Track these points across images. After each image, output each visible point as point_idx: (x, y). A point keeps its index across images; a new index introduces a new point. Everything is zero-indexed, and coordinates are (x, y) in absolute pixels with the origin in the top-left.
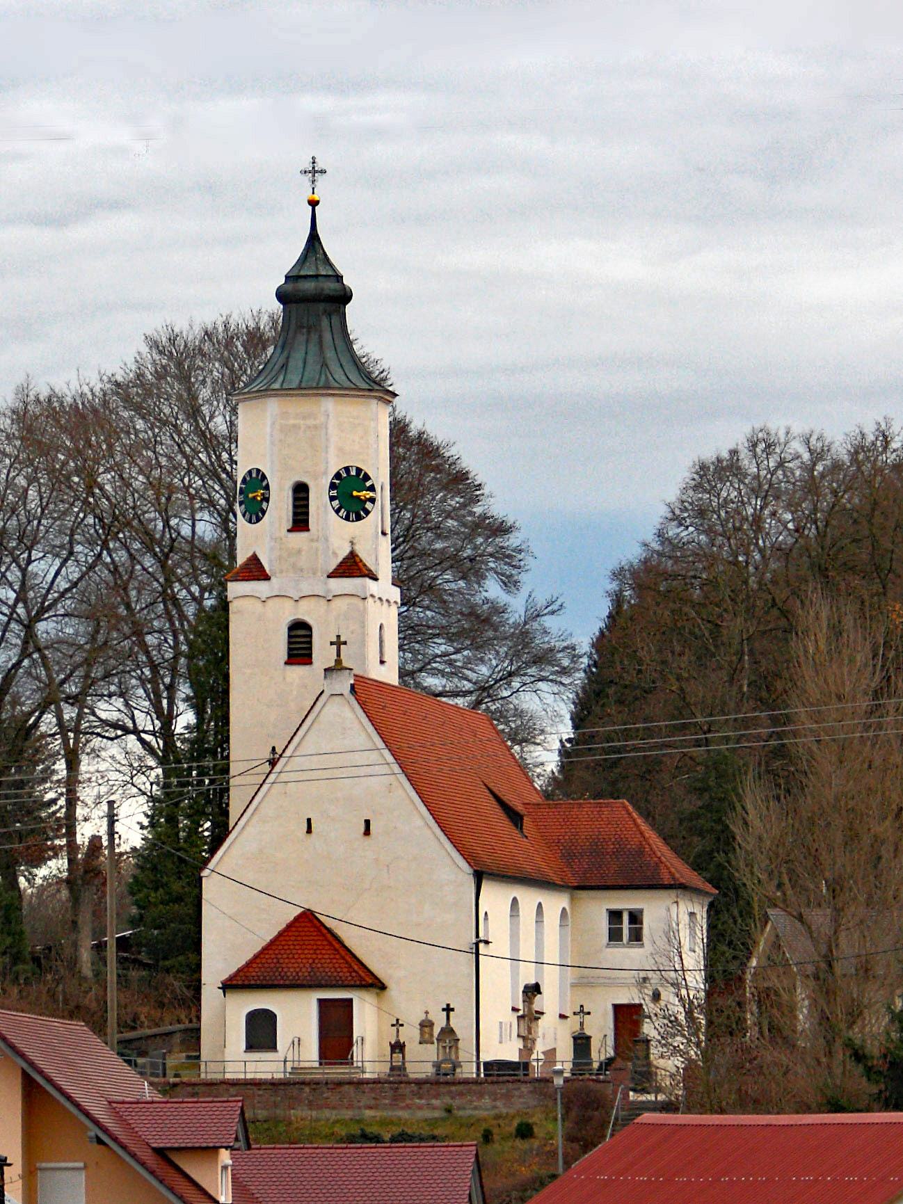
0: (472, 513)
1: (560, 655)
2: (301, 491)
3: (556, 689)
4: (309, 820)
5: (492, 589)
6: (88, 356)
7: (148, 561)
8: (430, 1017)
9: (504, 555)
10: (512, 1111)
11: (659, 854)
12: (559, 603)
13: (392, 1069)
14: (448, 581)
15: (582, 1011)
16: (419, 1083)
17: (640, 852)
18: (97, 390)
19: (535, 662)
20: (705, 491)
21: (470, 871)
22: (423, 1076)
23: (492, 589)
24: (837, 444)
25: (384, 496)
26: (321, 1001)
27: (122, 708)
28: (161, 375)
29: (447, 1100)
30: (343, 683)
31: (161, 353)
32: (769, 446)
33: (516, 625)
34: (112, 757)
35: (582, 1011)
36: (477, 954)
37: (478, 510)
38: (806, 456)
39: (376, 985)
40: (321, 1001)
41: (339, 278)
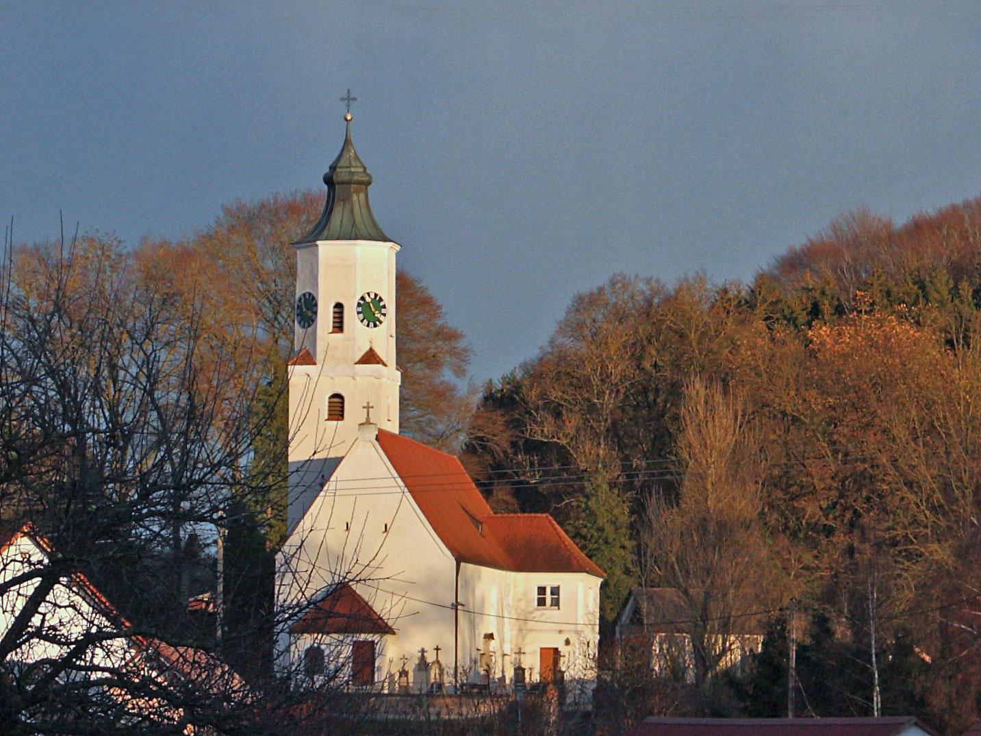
0: (434, 325)
2: (339, 306)
5: (447, 375)
9: (454, 352)
21: (453, 559)
23: (447, 375)
32: (624, 286)
36: (457, 610)
37: (439, 322)
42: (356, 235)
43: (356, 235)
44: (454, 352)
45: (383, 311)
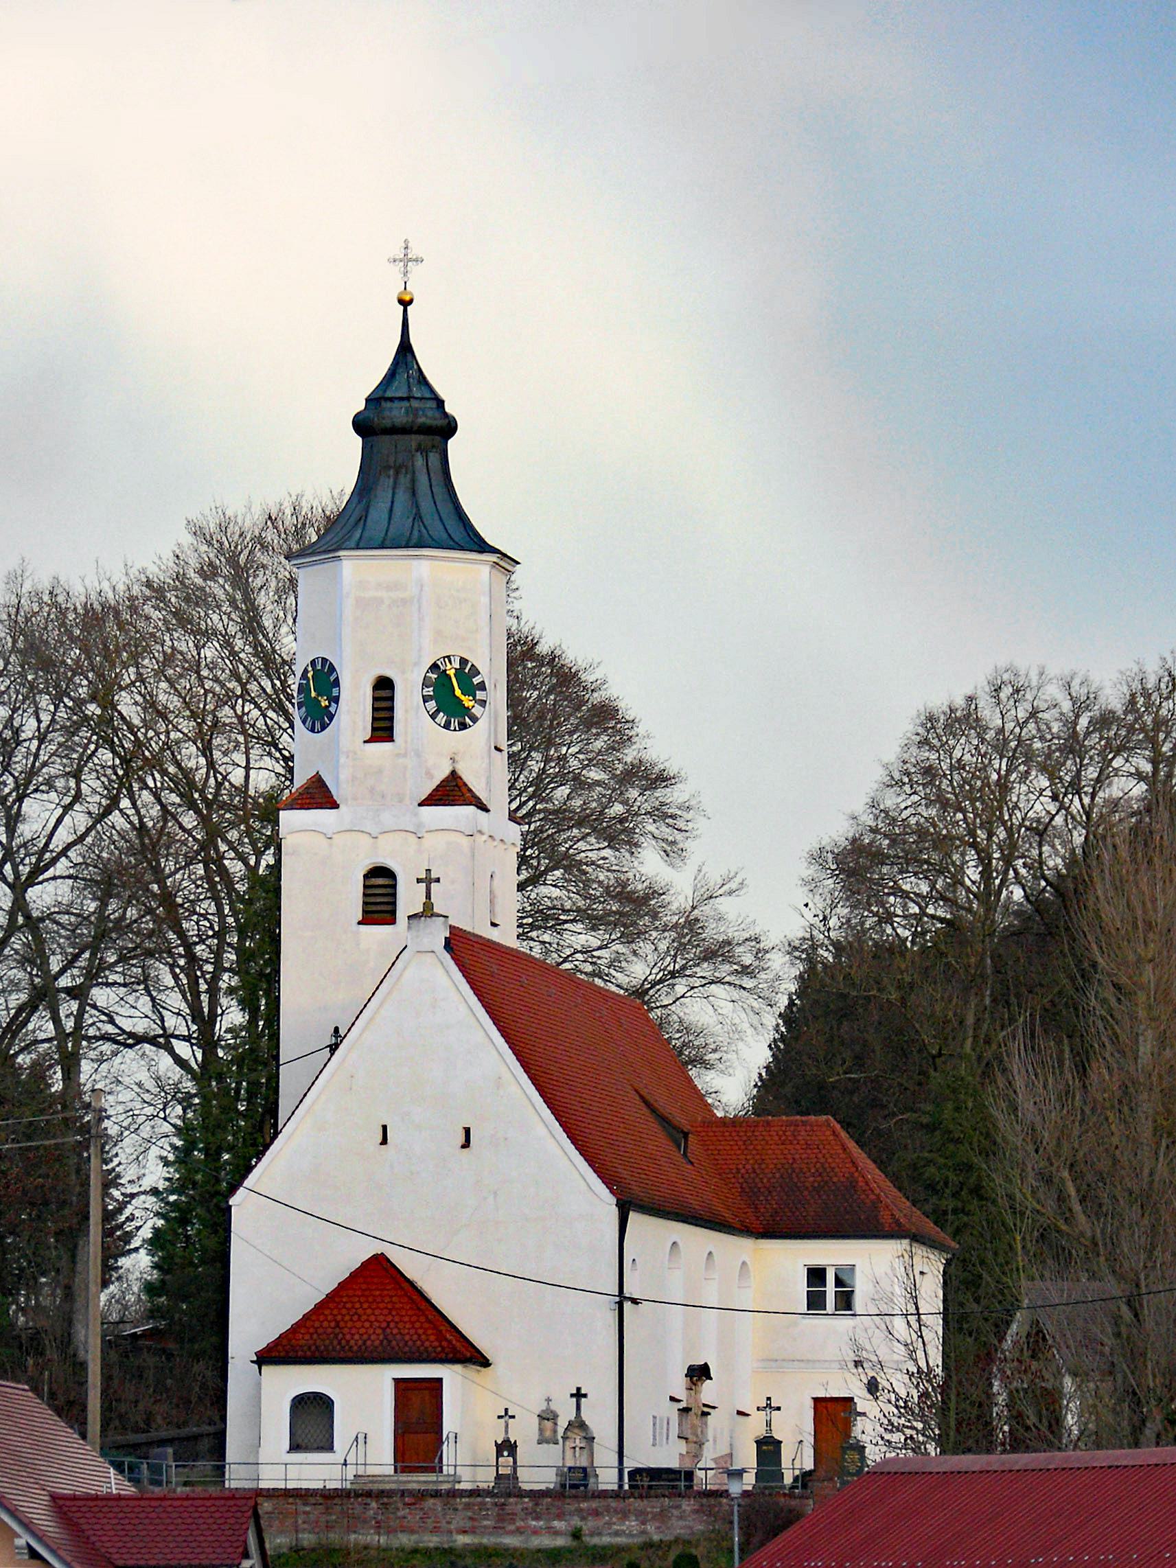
1: (741, 949)
2: (384, 686)
3: (736, 993)
4: (385, 1128)
6: (107, 548)
7: (189, 820)
8: (553, 1406)
9: (661, 814)
10: (669, 1537)
11: (877, 1191)
12: (738, 880)
13: (499, 1477)
14: (590, 849)
15: (769, 1406)
16: (536, 1495)
17: (853, 1185)
18: (121, 588)
19: (705, 959)
20: (932, 748)
21: (613, 1200)
22: (543, 1487)
24: (1108, 691)
25: (497, 695)
26: (398, 1382)
27: (150, 1014)
28: (209, 572)
29: (576, 1522)
30: (436, 934)
31: (210, 544)
33: (679, 913)
34: (140, 1085)
35: (769, 1406)
38: (1066, 706)
39: (473, 1357)
40: (398, 1382)
41: (440, 403)
42: (421, 536)
43: (421, 536)
44: (661, 814)
45: (480, 695)
